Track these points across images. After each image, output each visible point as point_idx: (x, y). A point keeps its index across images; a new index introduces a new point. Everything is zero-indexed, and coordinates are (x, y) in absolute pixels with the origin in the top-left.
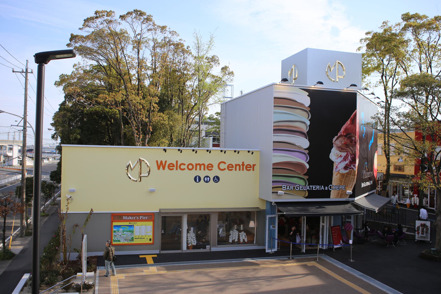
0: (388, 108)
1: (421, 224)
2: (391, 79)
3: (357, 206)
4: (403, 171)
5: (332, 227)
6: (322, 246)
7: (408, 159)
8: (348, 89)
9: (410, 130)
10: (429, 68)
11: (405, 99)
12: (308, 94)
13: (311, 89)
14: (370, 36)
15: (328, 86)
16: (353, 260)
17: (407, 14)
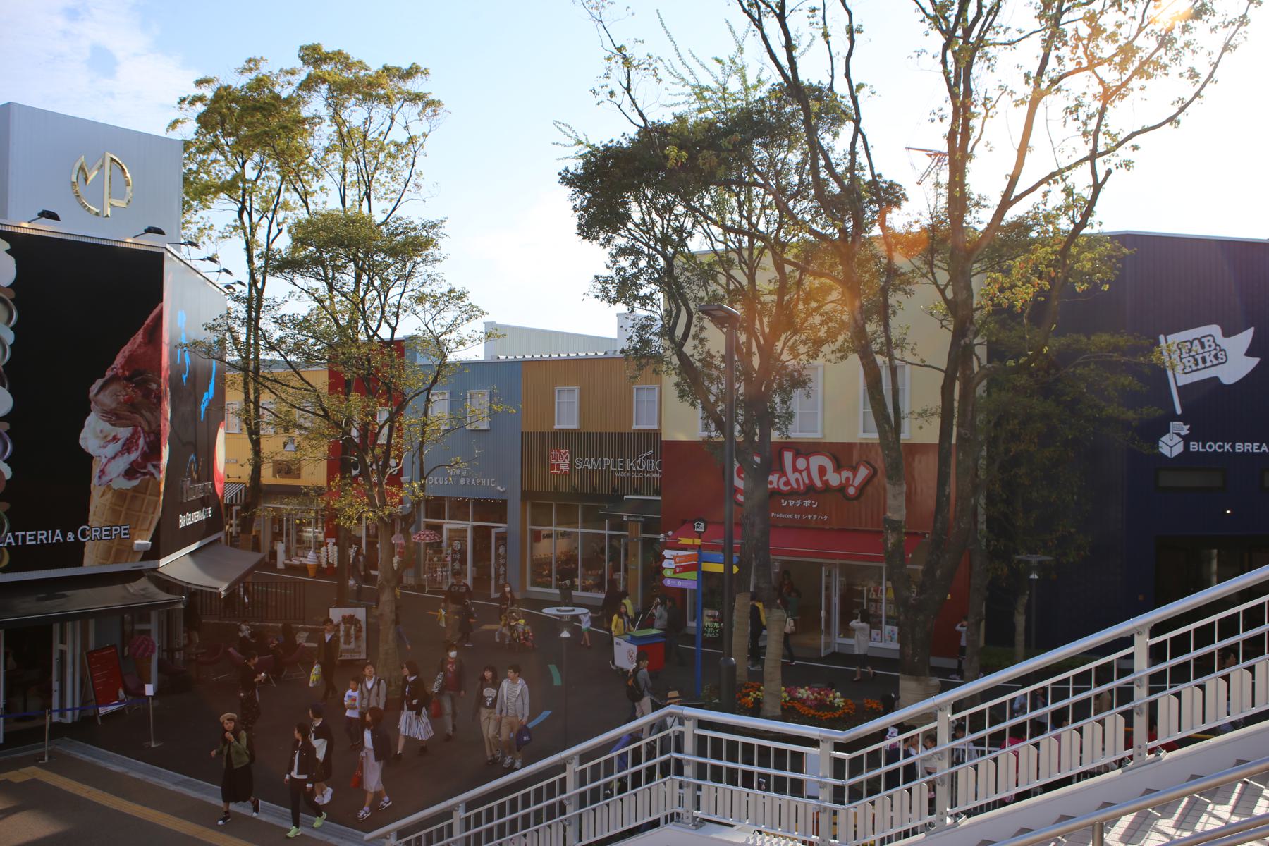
0: (255, 302)
1: (344, 617)
2: (265, 222)
3: (167, 584)
4: (299, 476)
5: (90, 654)
6: (62, 714)
7: (305, 444)
8: (138, 241)
9: (312, 365)
10: (366, 200)
11: (298, 279)
12: (8, 246)
13: (19, 230)
14: (208, 92)
15: (74, 226)
16: (156, 741)
17: (315, 48)
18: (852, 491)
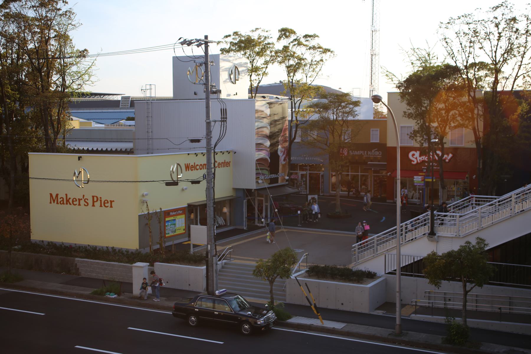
18: (447, 161)
